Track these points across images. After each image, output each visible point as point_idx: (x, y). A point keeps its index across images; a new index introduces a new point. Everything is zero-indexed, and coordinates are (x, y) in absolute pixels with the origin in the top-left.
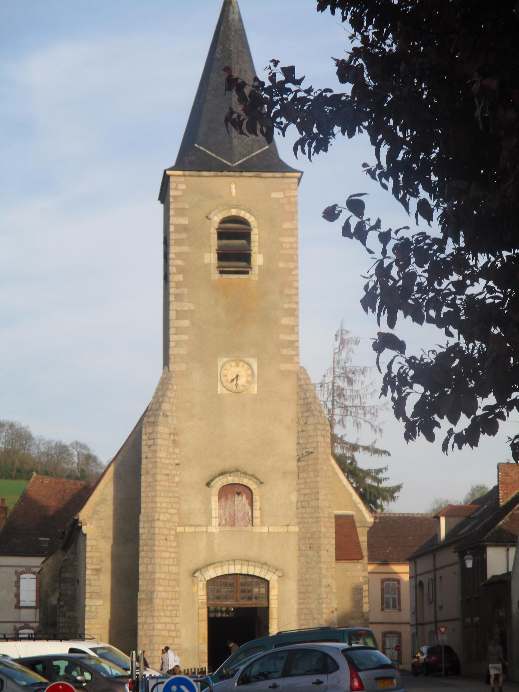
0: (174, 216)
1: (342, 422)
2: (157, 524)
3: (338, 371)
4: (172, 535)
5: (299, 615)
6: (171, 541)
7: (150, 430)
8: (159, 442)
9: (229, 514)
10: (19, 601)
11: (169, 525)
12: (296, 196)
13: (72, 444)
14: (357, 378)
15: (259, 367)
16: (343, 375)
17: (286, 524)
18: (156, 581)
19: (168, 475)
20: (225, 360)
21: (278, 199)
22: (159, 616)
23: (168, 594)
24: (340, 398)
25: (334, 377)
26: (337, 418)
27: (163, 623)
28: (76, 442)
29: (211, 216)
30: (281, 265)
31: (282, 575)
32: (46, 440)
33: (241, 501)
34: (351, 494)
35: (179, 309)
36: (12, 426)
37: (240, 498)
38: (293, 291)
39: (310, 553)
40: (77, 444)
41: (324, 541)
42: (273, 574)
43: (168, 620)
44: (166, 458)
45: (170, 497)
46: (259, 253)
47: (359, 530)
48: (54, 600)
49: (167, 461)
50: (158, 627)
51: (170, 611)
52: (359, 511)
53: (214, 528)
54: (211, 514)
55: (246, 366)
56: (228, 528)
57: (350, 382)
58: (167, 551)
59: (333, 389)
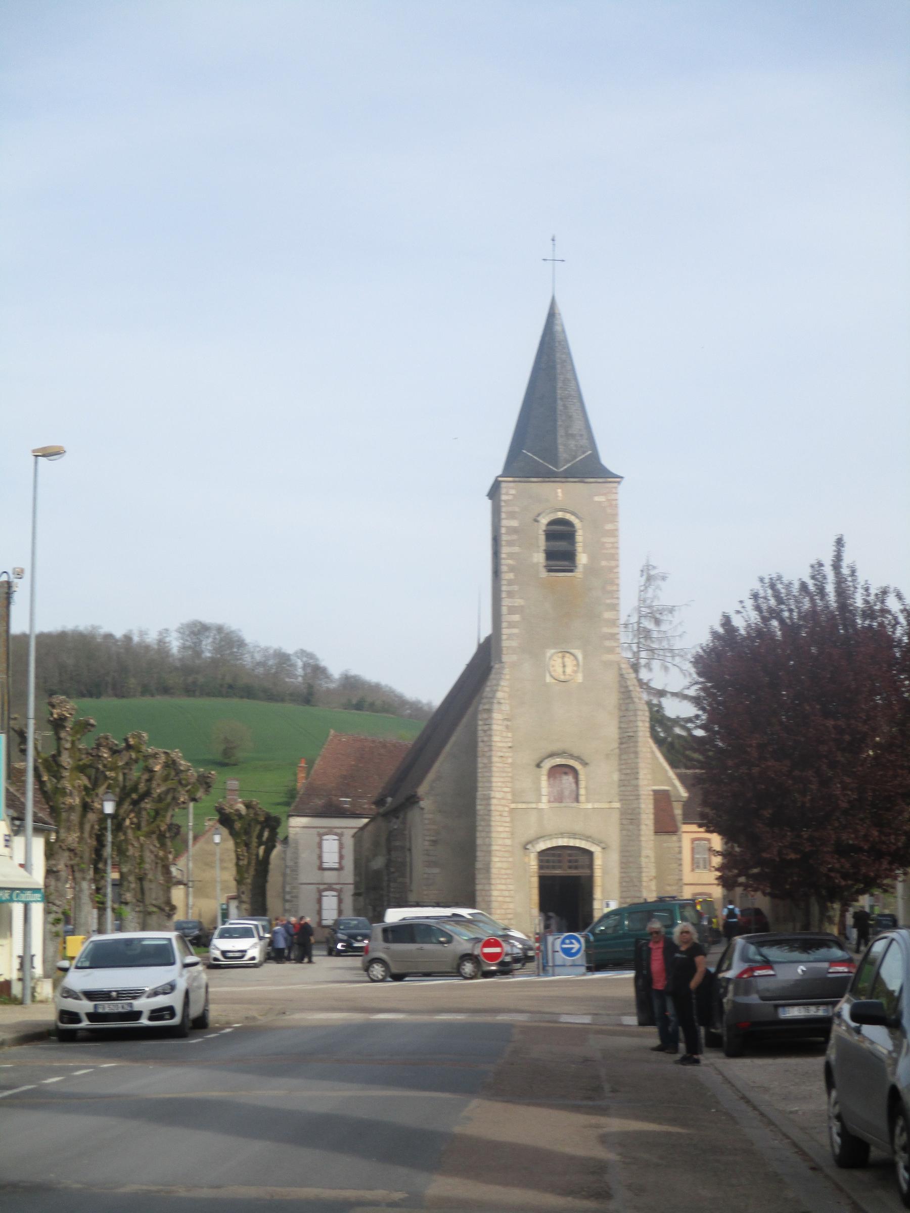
0: (506, 519)
1: (648, 666)
2: (494, 801)
3: (645, 611)
5: (621, 883)
7: (485, 716)
8: (495, 727)
10: (321, 862)
11: (503, 802)
12: (616, 500)
13: (296, 653)
14: (665, 617)
15: (584, 658)
16: (650, 615)
17: (609, 800)
20: (553, 651)
21: (600, 502)
24: (646, 640)
26: (643, 662)
28: (301, 650)
29: (539, 518)
30: (604, 563)
32: (262, 647)
33: (568, 780)
34: (666, 771)
35: (510, 605)
36: (220, 629)
38: (614, 588)
39: (631, 827)
40: (303, 653)
41: (644, 816)
43: (503, 887)
47: (675, 804)
48: (378, 863)
50: (495, 893)
52: (674, 786)
53: (544, 805)
55: (572, 657)
56: (556, 805)
57: (658, 622)
59: (638, 630)
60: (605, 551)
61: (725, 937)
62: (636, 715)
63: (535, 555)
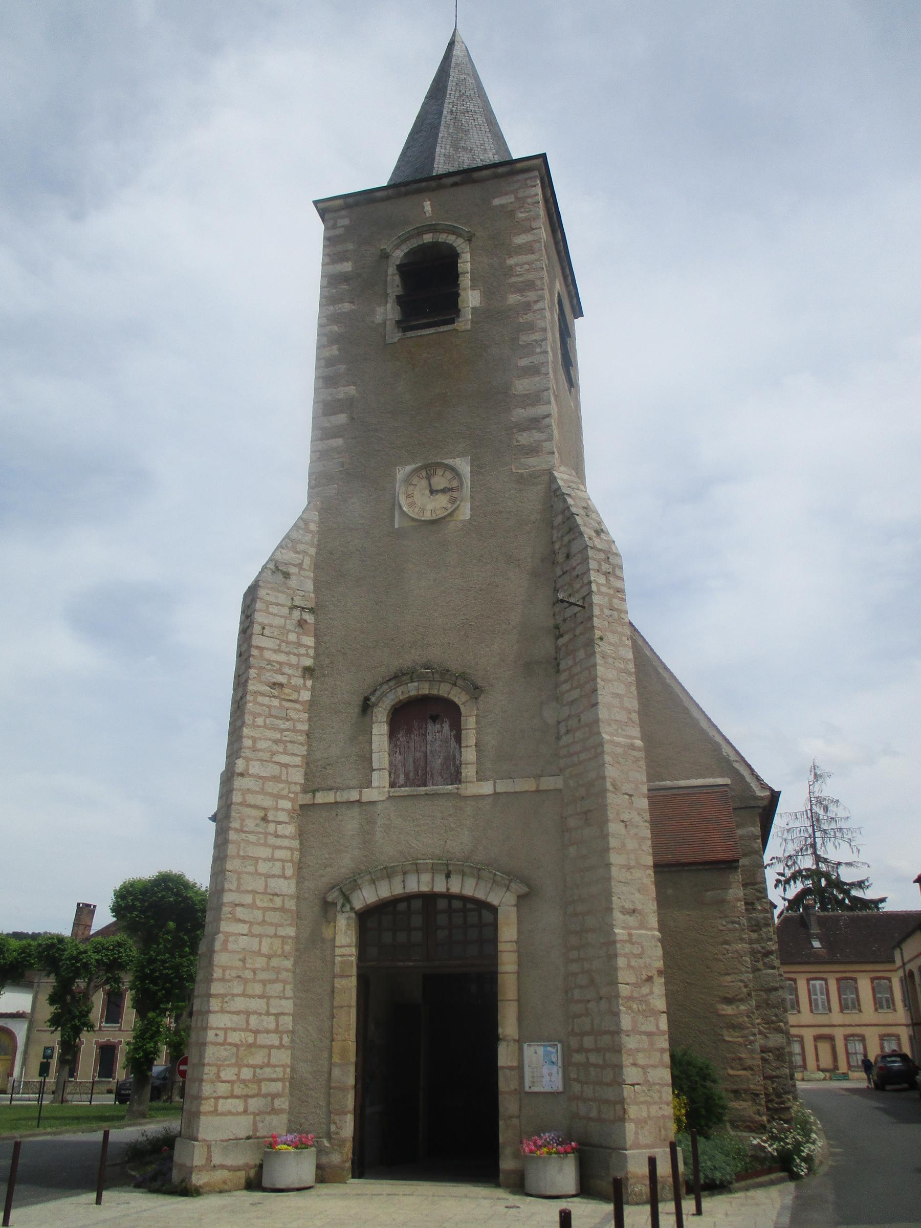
4: (283, 810)
6: (280, 823)
9: (414, 762)
18: (226, 909)
19: (281, 685)
20: (409, 468)
21: (502, 206)
22: (225, 995)
23: (260, 942)
25: (811, 805)
27: (238, 1013)
31: (526, 889)
33: (437, 733)
37: (438, 726)
42: (505, 889)
44: (278, 651)
45: (282, 731)
46: (473, 288)
49: (282, 658)
51: (264, 983)
54: (371, 763)
57: (826, 809)
58: (266, 845)
60: (514, 280)
61: (344, 203)
62: (586, 560)
63: (380, 310)
